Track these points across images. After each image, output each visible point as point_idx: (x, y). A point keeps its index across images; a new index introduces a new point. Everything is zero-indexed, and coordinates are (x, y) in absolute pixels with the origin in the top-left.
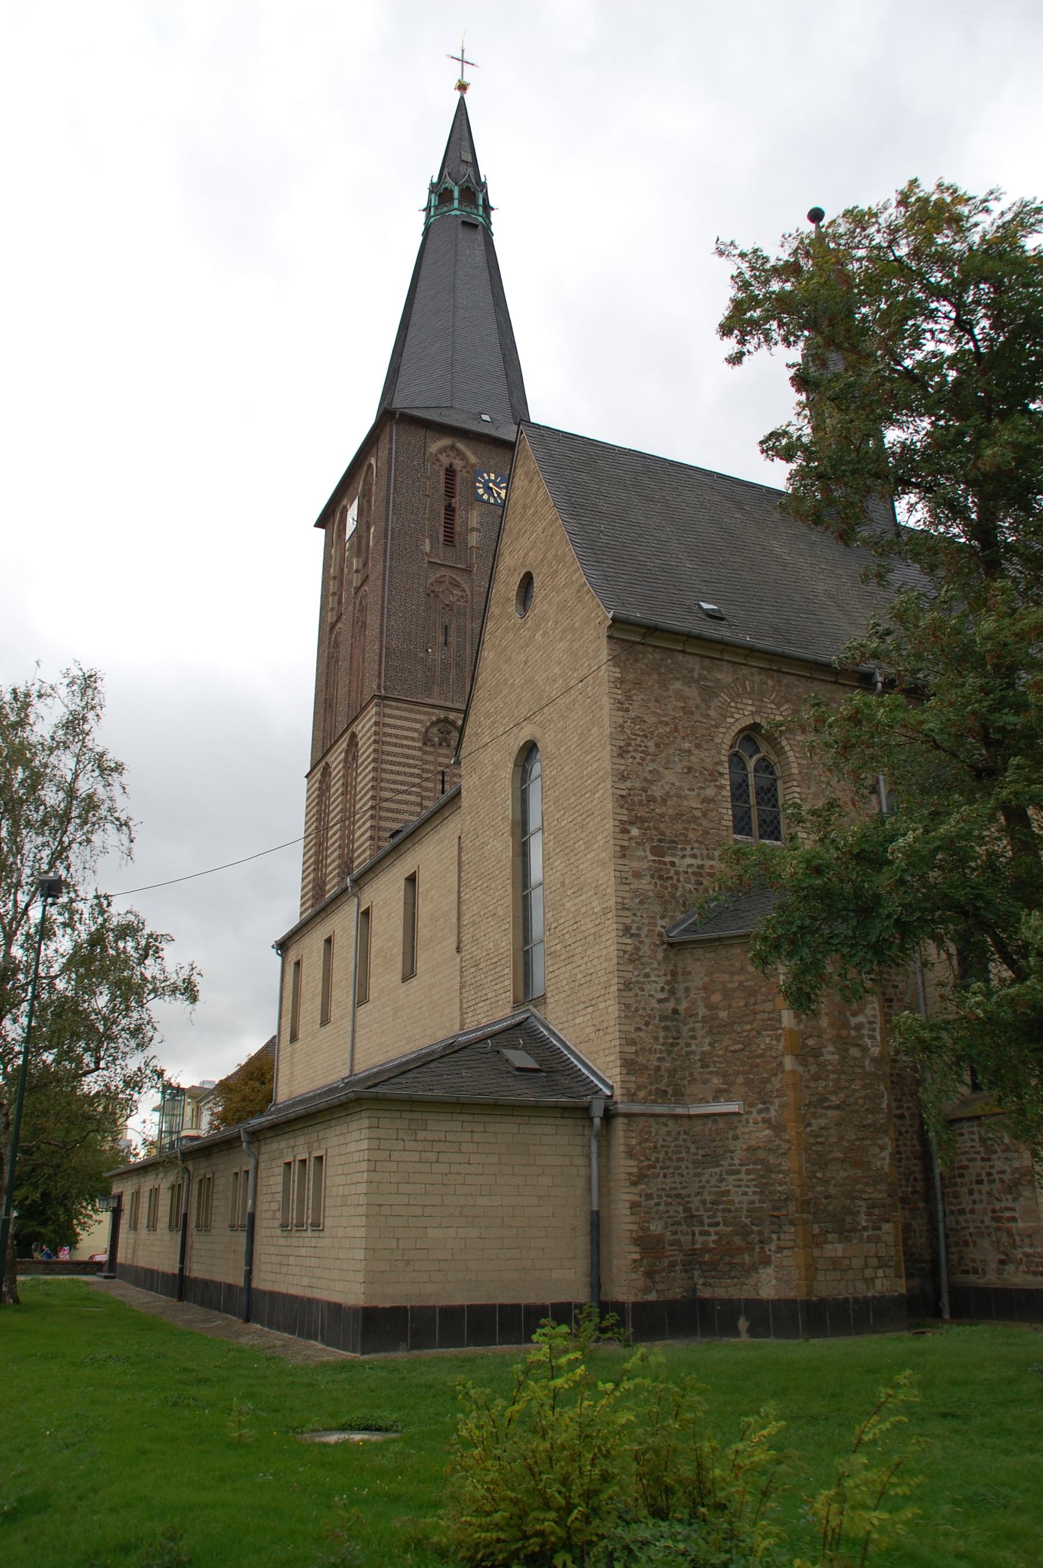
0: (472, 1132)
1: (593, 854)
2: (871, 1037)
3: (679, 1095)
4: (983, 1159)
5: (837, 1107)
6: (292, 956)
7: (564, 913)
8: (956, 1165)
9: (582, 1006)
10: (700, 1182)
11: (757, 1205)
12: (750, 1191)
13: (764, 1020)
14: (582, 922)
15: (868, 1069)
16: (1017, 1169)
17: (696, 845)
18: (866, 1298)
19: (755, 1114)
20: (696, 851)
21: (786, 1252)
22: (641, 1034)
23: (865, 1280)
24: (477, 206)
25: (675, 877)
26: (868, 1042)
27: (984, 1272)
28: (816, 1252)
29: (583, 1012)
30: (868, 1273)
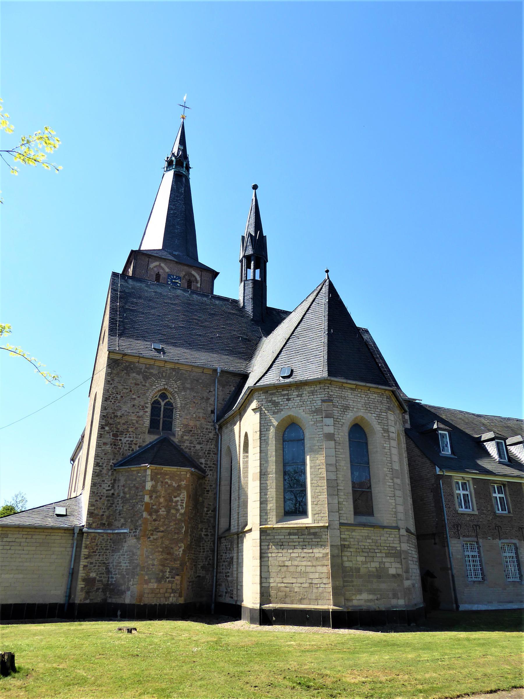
0: (26, 538)
3: (110, 525)
5: (162, 532)
11: (129, 567)
15: (178, 517)
17: (131, 433)
18: (164, 605)
23: (165, 597)
24: (183, 167)
28: (145, 586)
30: (167, 595)
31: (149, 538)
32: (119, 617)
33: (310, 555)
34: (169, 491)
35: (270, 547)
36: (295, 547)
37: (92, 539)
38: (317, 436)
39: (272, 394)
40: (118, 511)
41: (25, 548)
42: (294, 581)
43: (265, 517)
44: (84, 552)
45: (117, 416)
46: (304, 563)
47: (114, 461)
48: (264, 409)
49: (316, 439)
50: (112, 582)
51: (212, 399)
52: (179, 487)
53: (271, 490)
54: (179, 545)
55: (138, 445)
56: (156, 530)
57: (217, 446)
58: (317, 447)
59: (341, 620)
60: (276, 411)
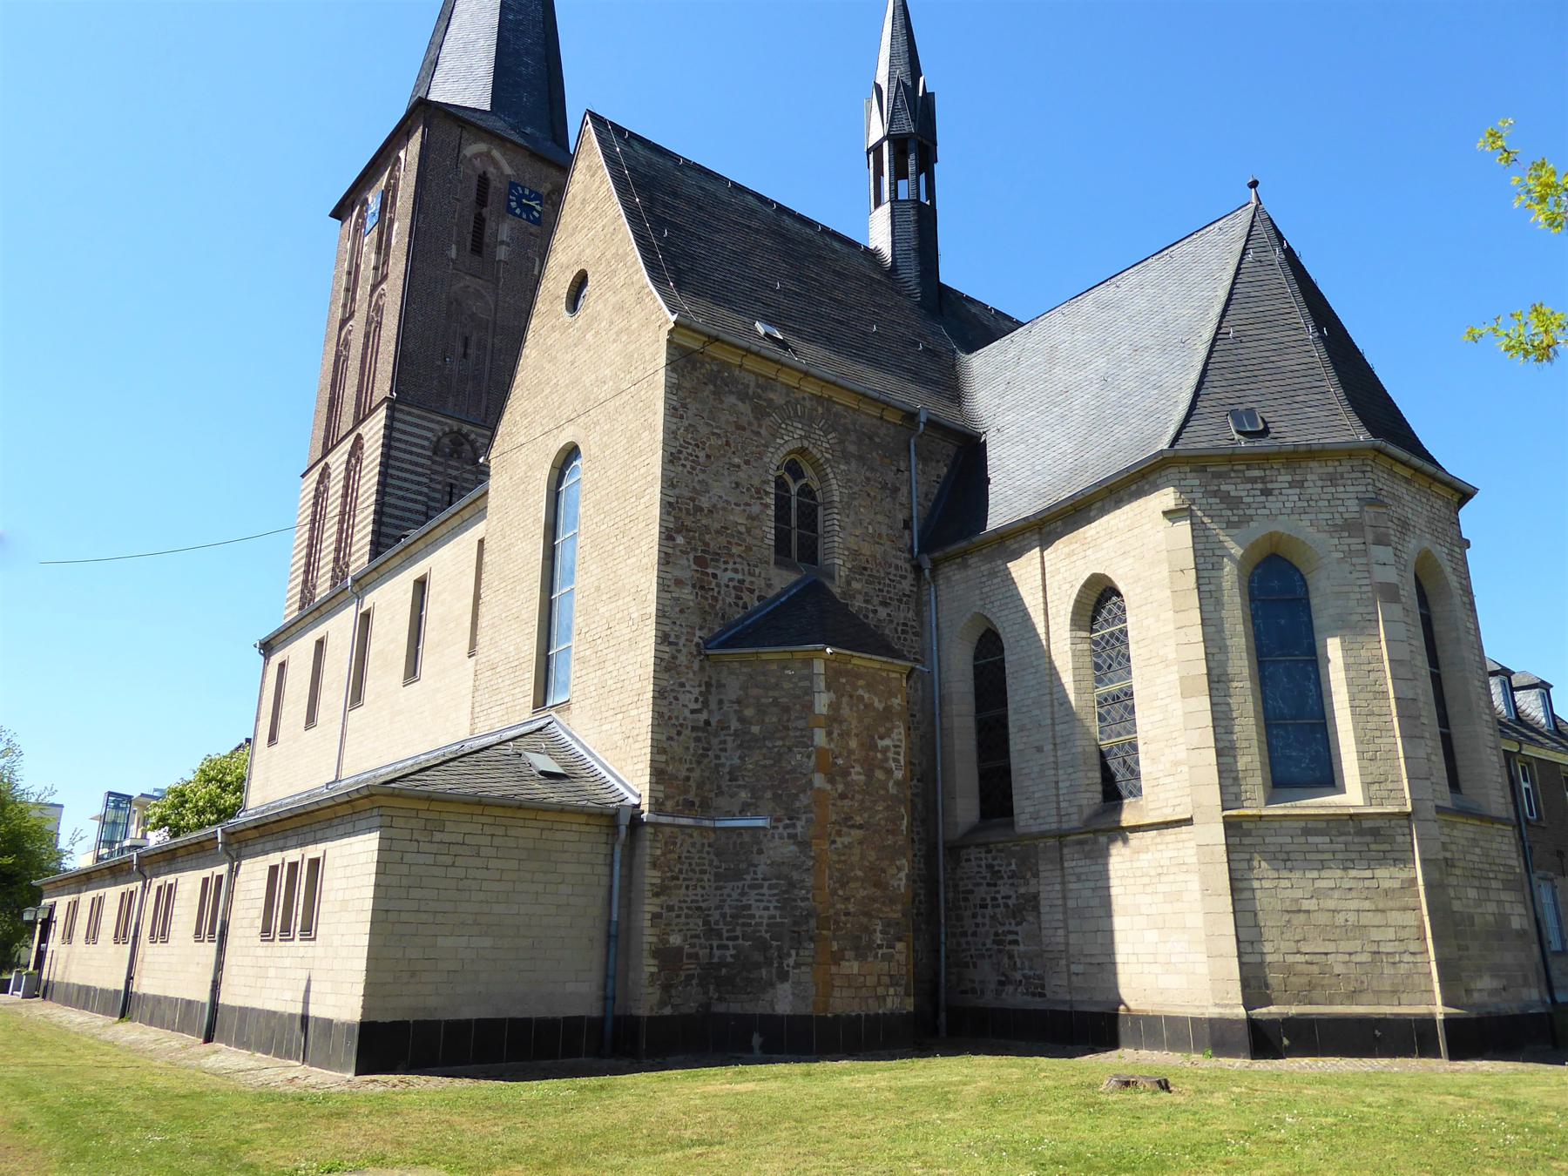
2: (895, 760)
5: (860, 827)
6: (276, 659)
12: (771, 905)
23: (878, 998)
27: (982, 992)
28: (834, 969)
30: (880, 991)
31: (834, 842)
32: (757, 1052)
33: (1367, 883)
34: (867, 721)
35: (1256, 863)
36: (1323, 865)
41: (492, 863)
42: (1330, 947)
43: (1234, 789)
44: (651, 877)
45: (701, 509)
46: (1354, 905)
47: (704, 633)
49: (1353, 596)
50: (723, 957)
51: (904, 490)
52: (887, 715)
57: (919, 613)
58: (1355, 618)
59: (1473, 1037)
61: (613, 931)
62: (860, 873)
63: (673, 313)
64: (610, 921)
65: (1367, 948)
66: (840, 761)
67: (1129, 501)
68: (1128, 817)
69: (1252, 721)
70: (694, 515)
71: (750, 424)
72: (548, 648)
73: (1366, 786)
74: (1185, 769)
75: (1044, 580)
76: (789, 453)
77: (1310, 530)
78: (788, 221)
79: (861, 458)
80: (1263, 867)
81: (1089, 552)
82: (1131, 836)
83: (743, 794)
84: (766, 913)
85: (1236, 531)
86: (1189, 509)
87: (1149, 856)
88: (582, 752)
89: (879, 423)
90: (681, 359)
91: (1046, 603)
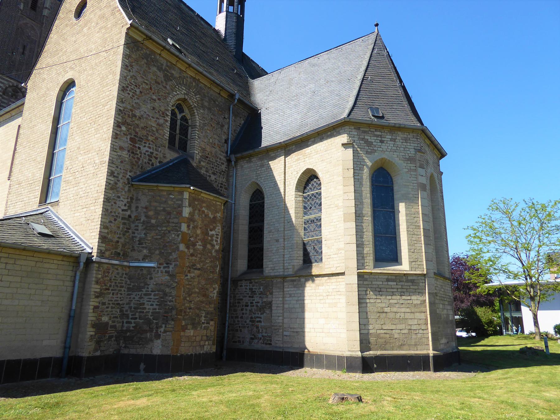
0: (6, 263)
1: (99, 135)
2: (216, 241)
4: (250, 297)
5: (199, 269)
7: (77, 162)
8: (237, 298)
9: (80, 207)
10: (130, 298)
11: (157, 310)
12: (155, 304)
13: (173, 226)
14: (87, 167)
16: (265, 302)
17: (151, 143)
18: (200, 354)
19: (162, 268)
20: (150, 145)
21: (168, 333)
22: (112, 224)
23: (200, 346)
25: (140, 155)
26: (215, 243)
28: (182, 334)
29: (80, 211)
31: (187, 276)
32: (142, 373)
33: (409, 301)
35: (368, 292)
36: (393, 294)
37: (104, 272)
38: (412, 184)
39: (364, 132)
40: (137, 239)
42: (393, 327)
44: (95, 288)
45: (135, 116)
46: (403, 310)
48: (356, 146)
51: (226, 127)
53: (367, 233)
54: (214, 286)
55: (159, 160)
56: (193, 266)
57: (227, 180)
58: (411, 196)
60: (370, 150)
61: (72, 314)
62: (197, 290)
63: (130, 20)
64: (71, 309)
65: (407, 327)
66: (192, 239)
67: (327, 139)
68: (315, 270)
69: (371, 234)
70: (132, 118)
71: (162, 82)
72: (50, 176)
73: (411, 262)
74: (343, 252)
75: (285, 170)
76: (179, 100)
77: (397, 159)
78: (183, 6)
79: (209, 109)
80: (371, 294)
81: (306, 159)
82: (316, 279)
83: (145, 251)
84: (151, 307)
85: (370, 156)
86: (352, 144)
87: (323, 287)
88: (63, 226)
89: (218, 95)
90: (132, 44)
91: (285, 180)
